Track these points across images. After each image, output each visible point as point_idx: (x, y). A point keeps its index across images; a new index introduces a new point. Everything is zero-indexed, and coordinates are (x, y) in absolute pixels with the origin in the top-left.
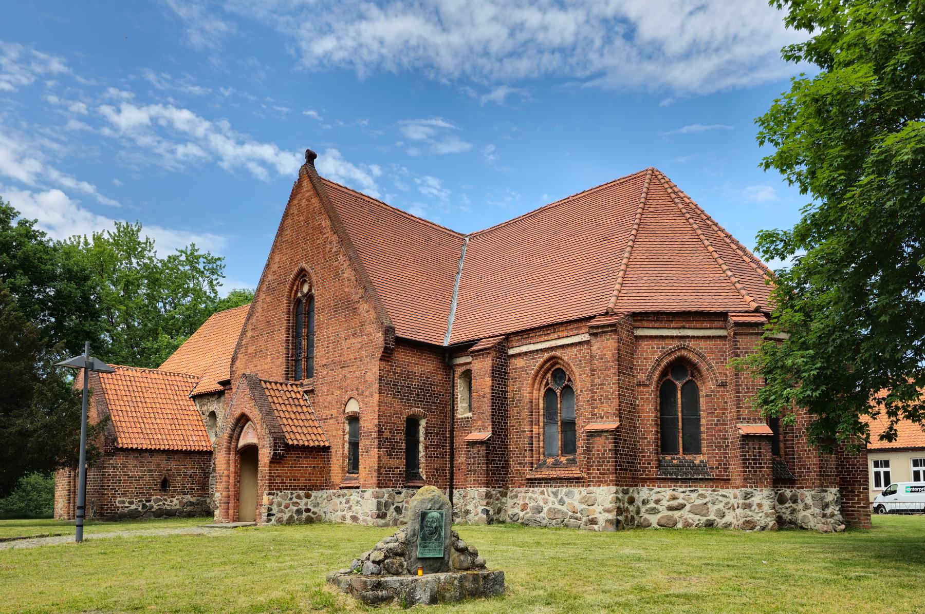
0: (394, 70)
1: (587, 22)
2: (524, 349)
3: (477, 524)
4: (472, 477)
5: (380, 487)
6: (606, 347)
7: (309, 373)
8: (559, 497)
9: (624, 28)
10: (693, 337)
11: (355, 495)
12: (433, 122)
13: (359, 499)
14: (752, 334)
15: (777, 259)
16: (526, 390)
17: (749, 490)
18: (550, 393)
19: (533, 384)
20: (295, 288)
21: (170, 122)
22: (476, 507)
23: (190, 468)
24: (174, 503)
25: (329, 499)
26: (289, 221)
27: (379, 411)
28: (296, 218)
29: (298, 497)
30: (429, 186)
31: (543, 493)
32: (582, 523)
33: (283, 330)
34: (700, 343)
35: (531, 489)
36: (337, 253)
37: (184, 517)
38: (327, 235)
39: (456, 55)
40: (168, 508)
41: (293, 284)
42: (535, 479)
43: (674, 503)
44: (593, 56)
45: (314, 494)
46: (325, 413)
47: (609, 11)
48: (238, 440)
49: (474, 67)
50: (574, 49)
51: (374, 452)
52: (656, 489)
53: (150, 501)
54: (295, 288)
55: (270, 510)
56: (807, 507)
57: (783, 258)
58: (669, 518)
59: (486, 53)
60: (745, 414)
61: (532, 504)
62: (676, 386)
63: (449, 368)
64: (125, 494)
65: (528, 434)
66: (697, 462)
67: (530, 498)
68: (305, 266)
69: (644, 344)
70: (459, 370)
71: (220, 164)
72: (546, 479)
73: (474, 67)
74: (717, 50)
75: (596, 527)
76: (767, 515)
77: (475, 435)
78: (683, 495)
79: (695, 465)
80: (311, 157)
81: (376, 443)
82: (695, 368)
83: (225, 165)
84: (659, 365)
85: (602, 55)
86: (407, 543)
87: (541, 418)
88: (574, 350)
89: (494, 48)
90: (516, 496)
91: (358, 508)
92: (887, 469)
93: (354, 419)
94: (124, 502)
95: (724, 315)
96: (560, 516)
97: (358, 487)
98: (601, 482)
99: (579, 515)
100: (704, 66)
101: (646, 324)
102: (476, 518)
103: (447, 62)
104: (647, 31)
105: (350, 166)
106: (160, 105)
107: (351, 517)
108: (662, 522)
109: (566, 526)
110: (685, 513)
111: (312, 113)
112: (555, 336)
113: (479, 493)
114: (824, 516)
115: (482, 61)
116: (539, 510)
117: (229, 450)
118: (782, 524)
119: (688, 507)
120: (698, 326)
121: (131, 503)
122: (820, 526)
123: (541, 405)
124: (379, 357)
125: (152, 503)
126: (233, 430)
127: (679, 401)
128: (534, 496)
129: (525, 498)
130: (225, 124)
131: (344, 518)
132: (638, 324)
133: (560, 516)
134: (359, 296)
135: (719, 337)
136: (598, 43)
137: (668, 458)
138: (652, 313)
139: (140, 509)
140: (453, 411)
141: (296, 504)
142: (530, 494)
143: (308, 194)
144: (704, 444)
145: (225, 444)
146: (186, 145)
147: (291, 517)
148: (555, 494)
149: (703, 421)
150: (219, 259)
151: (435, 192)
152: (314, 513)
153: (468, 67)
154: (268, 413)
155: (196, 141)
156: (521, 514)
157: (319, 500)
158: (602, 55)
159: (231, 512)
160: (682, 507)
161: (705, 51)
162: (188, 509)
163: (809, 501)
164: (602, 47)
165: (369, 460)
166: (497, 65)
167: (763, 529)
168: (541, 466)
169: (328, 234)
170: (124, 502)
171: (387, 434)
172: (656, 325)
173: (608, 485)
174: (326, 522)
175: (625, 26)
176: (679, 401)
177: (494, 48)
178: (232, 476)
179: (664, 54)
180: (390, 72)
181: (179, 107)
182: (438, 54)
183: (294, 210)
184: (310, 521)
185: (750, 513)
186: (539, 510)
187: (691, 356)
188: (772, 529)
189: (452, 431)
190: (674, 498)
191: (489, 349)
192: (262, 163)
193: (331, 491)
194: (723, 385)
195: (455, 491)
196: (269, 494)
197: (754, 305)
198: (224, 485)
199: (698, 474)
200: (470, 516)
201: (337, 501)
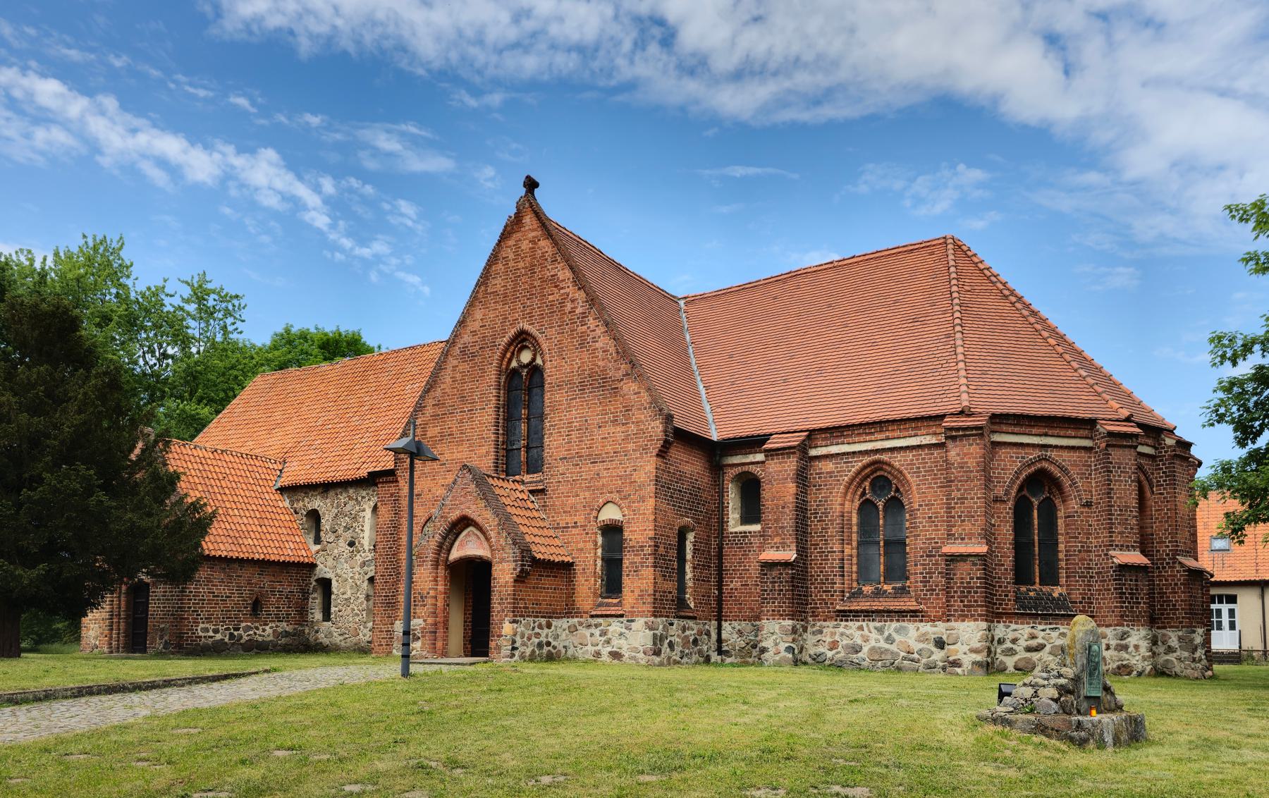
0: (351, 49)
1: (616, 17)
2: (834, 449)
3: (778, 664)
4: (770, 607)
5: (656, 616)
6: (967, 454)
7: (535, 465)
8: (886, 634)
9: (658, 31)
10: (1056, 447)
11: (615, 626)
12: (403, 127)
13: (623, 630)
14: (1126, 447)
15: (1228, 364)
16: (838, 501)
17: (1126, 629)
18: (866, 507)
19: (846, 494)
20: (508, 355)
21: (30, 95)
22: (776, 644)
23: (287, 586)
24: (267, 632)
25: (573, 630)
26: (500, 267)
27: (655, 520)
28: (511, 264)
29: (540, 627)
30: (402, 215)
31: (861, 628)
32: (921, 666)
33: (490, 410)
34: (1063, 452)
35: (843, 623)
36: (584, 315)
37: (279, 651)
38: (567, 290)
39: (438, 38)
40: (260, 639)
41: (506, 350)
42: (850, 611)
43: (1034, 643)
44: (621, 62)
45: (555, 622)
46: (564, 520)
47: (644, 9)
48: (449, 551)
49: (463, 58)
50: (596, 50)
51: (648, 573)
52: (1013, 626)
53: (238, 629)
54: (508, 355)
55: (514, 642)
56: (1170, 650)
57: (1235, 364)
58: (1028, 660)
59: (480, 42)
60: (1118, 540)
61: (845, 642)
62: (1032, 503)
63: (716, 469)
64: (209, 620)
65: (837, 555)
66: (1056, 595)
67: (842, 634)
68: (527, 327)
69: (1002, 452)
70: (731, 473)
71: (98, 158)
72: (867, 611)
73: (463, 58)
74: (775, 74)
75: (959, 670)
76: (1144, 659)
77: (770, 555)
78: (1042, 634)
79: (1054, 599)
80: (531, 185)
81: (651, 560)
82: (1056, 484)
83: (105, 161)
84: (1018, 478)
85: (632, 62)
86: (1076, 680)
87: (855, 537)
88: (910, 455)
89: (492, 35)
90: (821, 632)
91: (622, 642)
92: (1231, 606)
93: (612, 531)
94: (207, 630)
95: (1091, 423)
96: (889, 657)
97: (622, 616)
98: (966, 616)
99: (916, 656)
100: (762, 92)
101: (1004, 428)
102: (777, 658)
103: (427, 48)
104: (692, 37)
105: (290, 177)
106: (15, 69)
107: (610, 653)
108: (1020, 665)
109: (899, 669)
110: (1045, 655)
111: (242, 102)
112: (883, 436)
113: (782, 627)
114: (1194, 660)
115: (474, 51)
116: (856, 649)
117: (436, 564)
118: (1160, 672)
119: (1048, 648)
120: (1062, 433)
121: (216, 631)
122: (1189, 672)
123: (855, 520)
124: (655, 452)
125: (241, 632)
126: (444, 538)
127: (1036, 522)
128: (848, 632)
129: (833, 634)
130: (110, 103)
131: (598, 654)
132: (996, 427)
133: (889, 657)
134: (621, 373)
135: (1085, 448)
136: (627, 46)
137: (1023, 589)
138: (1014, 415)
139: (226, 640)
140: (722, 522)
141: (538, 635)
142: (841, 630)
143: (534, 234)
144: (1063, 573)
145: (431, 556)
146: (48, 129)
147: (533, 651)
148: (880, 630)
149: (1062, 547)
150: (237, 297)
151: (410, 223)
152: (554, 648)
153: (454, 56)
154: (506, 521)
155: (65, 125)
156: (830, 654)
157: (559, 631)
158: (632, 62)
159: (439, 644)
160: (1039, 648)
161: (761, 73)
162: (284, 641)
163: (1174, 642)
164: (633, 52)
165: (640, 580)
166: (494, 59)
167: (1140, 674)
168: (857, 594)
169: (570, 289)
170: (207, 630)
171: (661, 550)
172: (1017, 429)
173: (976, 620)
174: (568, 659)
175: (663, 29)
176: (1036, 522)
177: (492, 35)
178: (441, 598)
179: (709, 70)
180: (345, 53)
181: (44, 75)
182: (414, 34)
183: (509, 253)
184: (551, 658)
185: (1127, 656)
186: (856, 649)
187: (1052, 468)
188: (1149, 675)
189: (721, 548)
190: (1033, 637)
191: (790, 448)
192: (161, 162)
193: (576, 620)
194: (1088, 505)
195: (725, 625)
196: (514, 622)
197: (1125, 413)
198: (429, 608)
199: (1059, 609)
200: (766, 655)
201: (587, 633)
